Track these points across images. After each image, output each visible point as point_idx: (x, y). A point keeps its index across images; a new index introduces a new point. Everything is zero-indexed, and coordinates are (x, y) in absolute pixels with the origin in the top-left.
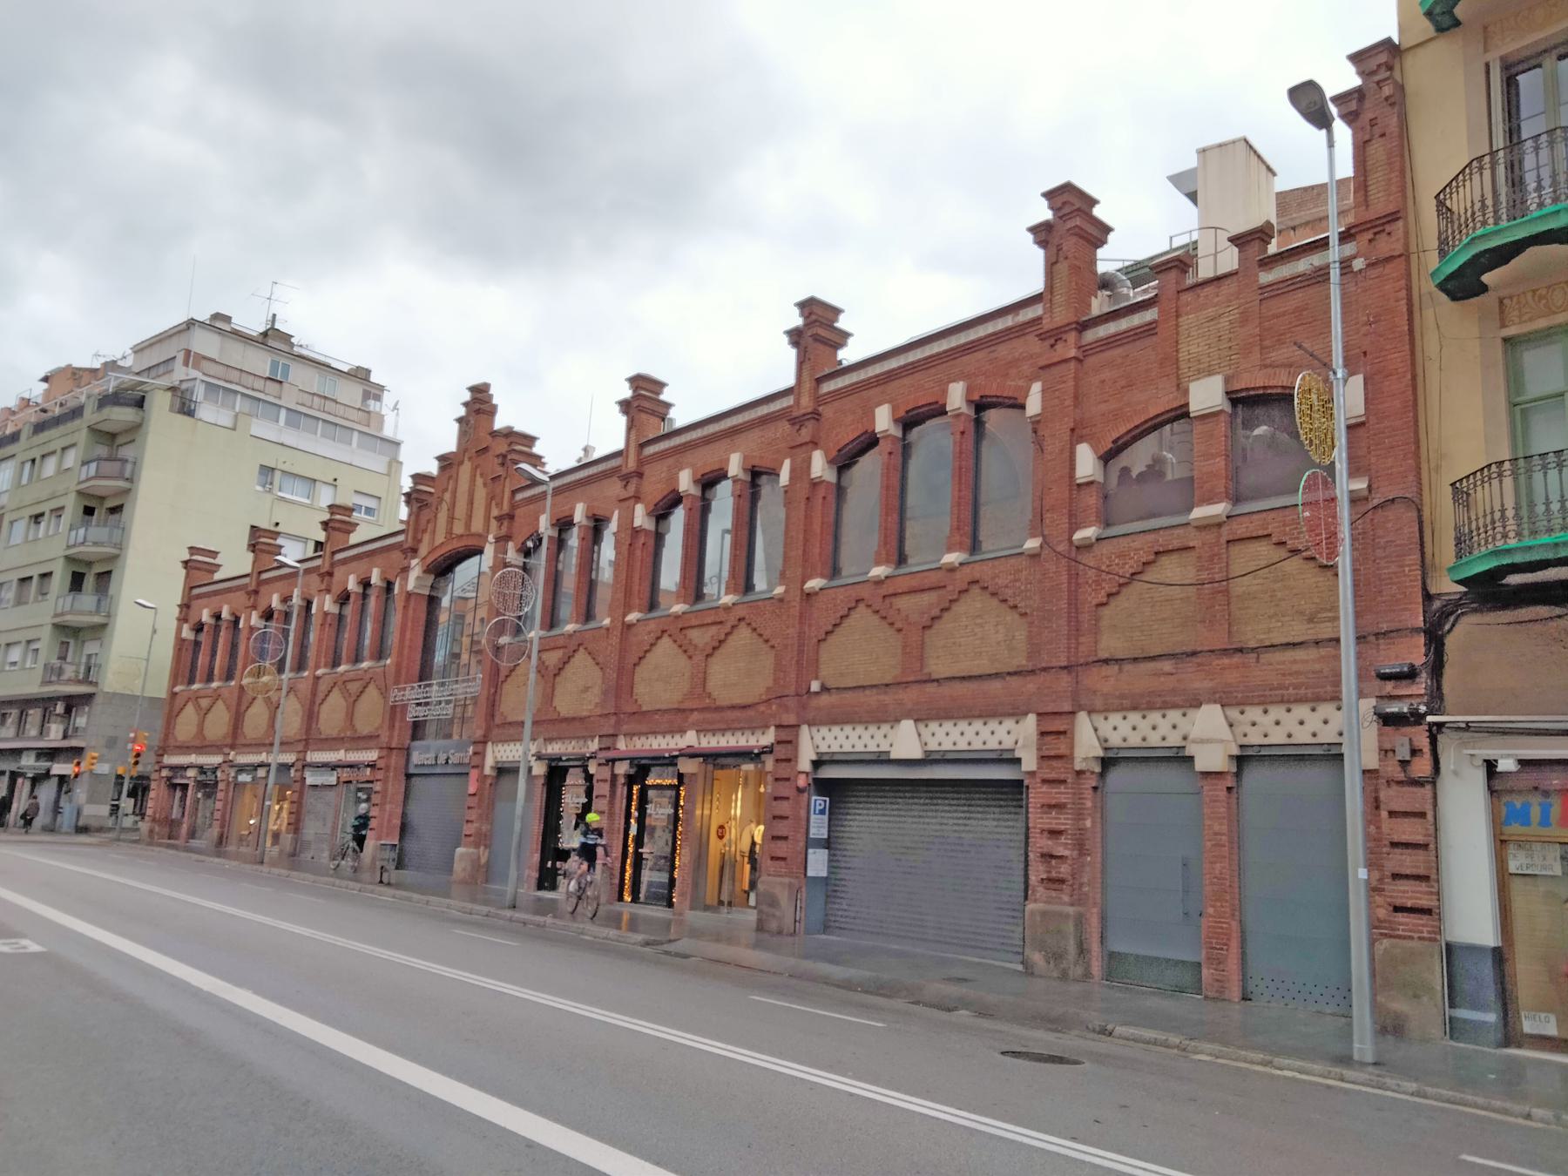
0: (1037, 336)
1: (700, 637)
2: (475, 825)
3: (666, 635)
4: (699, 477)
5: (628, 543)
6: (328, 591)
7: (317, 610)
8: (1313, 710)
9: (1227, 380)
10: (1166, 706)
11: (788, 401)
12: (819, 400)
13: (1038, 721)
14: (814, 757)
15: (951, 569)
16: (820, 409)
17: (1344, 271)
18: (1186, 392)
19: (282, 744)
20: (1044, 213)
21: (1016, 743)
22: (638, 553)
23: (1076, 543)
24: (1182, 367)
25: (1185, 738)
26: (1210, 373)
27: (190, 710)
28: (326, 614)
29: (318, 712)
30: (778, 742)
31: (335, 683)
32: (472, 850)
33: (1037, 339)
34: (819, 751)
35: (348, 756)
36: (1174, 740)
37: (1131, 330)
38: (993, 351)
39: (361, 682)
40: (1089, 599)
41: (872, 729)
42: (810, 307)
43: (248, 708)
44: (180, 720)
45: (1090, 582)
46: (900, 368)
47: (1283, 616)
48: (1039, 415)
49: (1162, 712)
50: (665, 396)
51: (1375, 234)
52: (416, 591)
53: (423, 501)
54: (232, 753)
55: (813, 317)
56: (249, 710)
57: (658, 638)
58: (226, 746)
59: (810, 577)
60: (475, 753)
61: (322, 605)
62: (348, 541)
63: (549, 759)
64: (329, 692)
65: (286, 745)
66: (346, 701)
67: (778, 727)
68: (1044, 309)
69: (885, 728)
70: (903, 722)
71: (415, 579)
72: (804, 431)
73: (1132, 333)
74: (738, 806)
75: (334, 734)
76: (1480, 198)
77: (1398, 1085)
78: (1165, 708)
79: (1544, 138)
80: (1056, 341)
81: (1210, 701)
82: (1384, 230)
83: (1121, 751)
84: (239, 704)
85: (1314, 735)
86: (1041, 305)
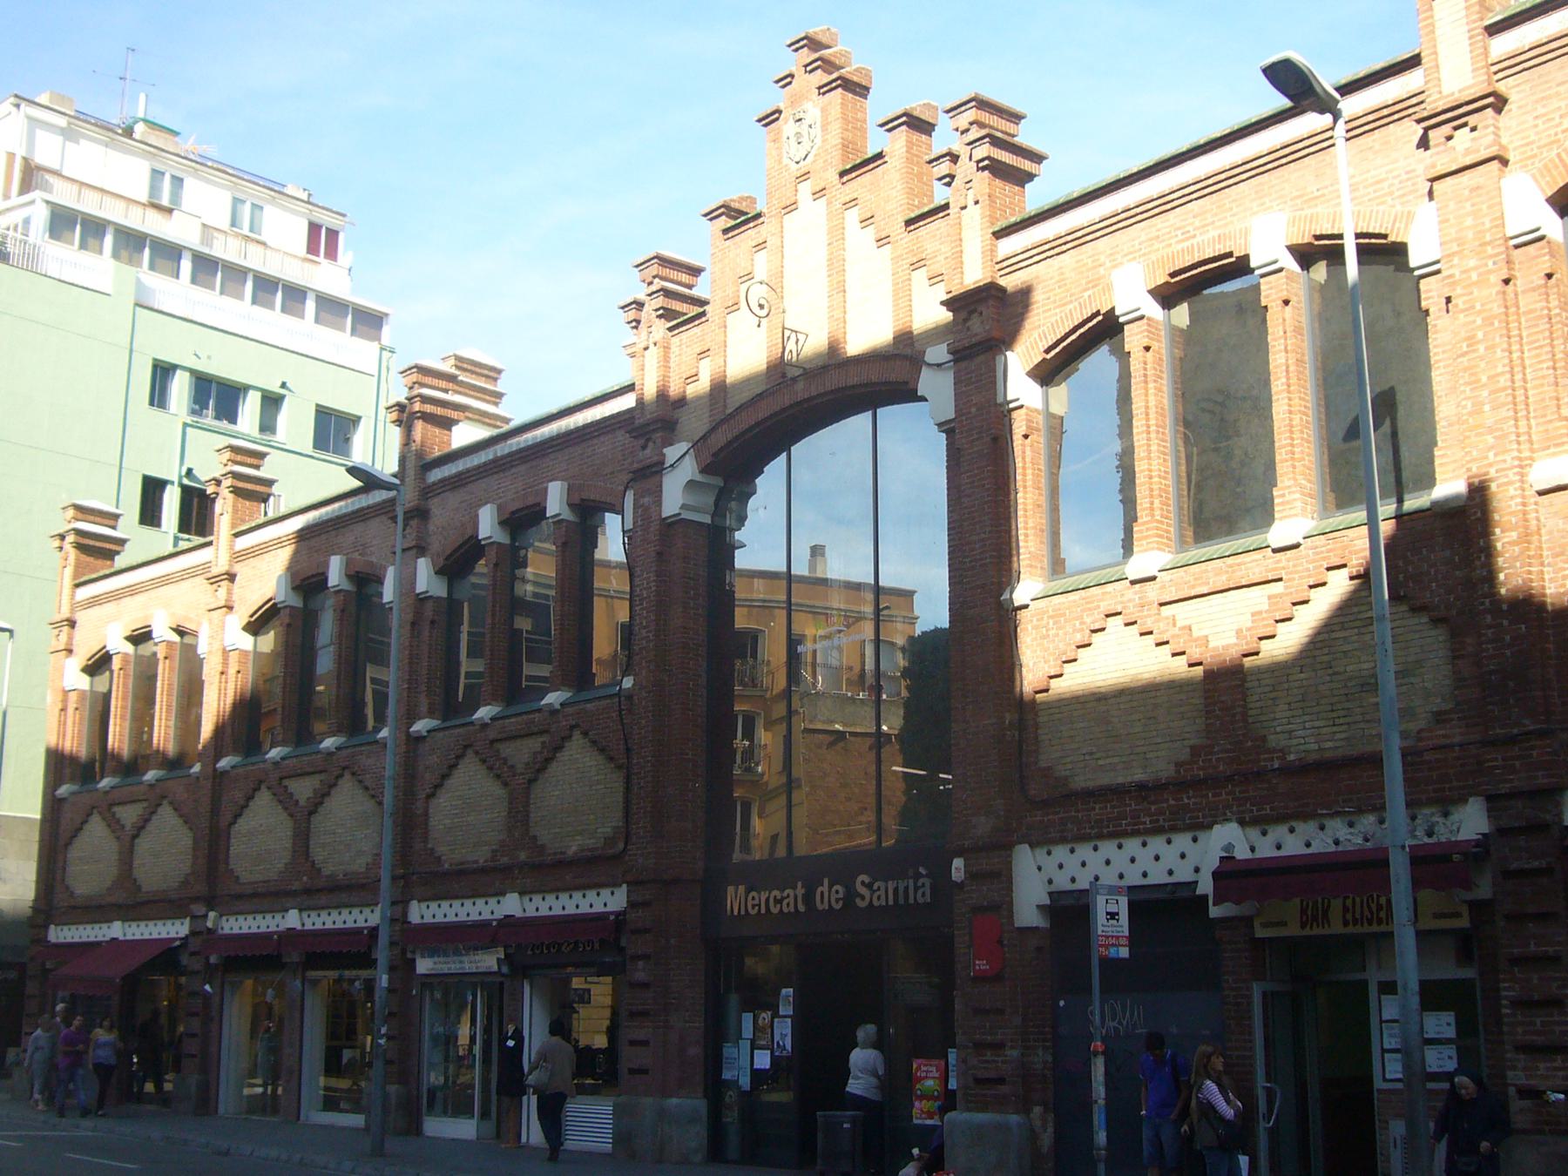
3: (470, 752)
4: (1162, 279)
6: (421, 549)
12: (427, 492)
27: (96, 828)
28: (422, 600)
29: (426, 814)
34: (1053, 888)
43: (237, 816)
44: (77, 851)
51: (1456, 128)
54: (212, 915)
56: (241, 821)
57: (459, 757)
58: (196, 899)
64: (453, 767)
74: (1536, 976)
75: (481, 856)
84: (215, 811)
85: (1170, 873)
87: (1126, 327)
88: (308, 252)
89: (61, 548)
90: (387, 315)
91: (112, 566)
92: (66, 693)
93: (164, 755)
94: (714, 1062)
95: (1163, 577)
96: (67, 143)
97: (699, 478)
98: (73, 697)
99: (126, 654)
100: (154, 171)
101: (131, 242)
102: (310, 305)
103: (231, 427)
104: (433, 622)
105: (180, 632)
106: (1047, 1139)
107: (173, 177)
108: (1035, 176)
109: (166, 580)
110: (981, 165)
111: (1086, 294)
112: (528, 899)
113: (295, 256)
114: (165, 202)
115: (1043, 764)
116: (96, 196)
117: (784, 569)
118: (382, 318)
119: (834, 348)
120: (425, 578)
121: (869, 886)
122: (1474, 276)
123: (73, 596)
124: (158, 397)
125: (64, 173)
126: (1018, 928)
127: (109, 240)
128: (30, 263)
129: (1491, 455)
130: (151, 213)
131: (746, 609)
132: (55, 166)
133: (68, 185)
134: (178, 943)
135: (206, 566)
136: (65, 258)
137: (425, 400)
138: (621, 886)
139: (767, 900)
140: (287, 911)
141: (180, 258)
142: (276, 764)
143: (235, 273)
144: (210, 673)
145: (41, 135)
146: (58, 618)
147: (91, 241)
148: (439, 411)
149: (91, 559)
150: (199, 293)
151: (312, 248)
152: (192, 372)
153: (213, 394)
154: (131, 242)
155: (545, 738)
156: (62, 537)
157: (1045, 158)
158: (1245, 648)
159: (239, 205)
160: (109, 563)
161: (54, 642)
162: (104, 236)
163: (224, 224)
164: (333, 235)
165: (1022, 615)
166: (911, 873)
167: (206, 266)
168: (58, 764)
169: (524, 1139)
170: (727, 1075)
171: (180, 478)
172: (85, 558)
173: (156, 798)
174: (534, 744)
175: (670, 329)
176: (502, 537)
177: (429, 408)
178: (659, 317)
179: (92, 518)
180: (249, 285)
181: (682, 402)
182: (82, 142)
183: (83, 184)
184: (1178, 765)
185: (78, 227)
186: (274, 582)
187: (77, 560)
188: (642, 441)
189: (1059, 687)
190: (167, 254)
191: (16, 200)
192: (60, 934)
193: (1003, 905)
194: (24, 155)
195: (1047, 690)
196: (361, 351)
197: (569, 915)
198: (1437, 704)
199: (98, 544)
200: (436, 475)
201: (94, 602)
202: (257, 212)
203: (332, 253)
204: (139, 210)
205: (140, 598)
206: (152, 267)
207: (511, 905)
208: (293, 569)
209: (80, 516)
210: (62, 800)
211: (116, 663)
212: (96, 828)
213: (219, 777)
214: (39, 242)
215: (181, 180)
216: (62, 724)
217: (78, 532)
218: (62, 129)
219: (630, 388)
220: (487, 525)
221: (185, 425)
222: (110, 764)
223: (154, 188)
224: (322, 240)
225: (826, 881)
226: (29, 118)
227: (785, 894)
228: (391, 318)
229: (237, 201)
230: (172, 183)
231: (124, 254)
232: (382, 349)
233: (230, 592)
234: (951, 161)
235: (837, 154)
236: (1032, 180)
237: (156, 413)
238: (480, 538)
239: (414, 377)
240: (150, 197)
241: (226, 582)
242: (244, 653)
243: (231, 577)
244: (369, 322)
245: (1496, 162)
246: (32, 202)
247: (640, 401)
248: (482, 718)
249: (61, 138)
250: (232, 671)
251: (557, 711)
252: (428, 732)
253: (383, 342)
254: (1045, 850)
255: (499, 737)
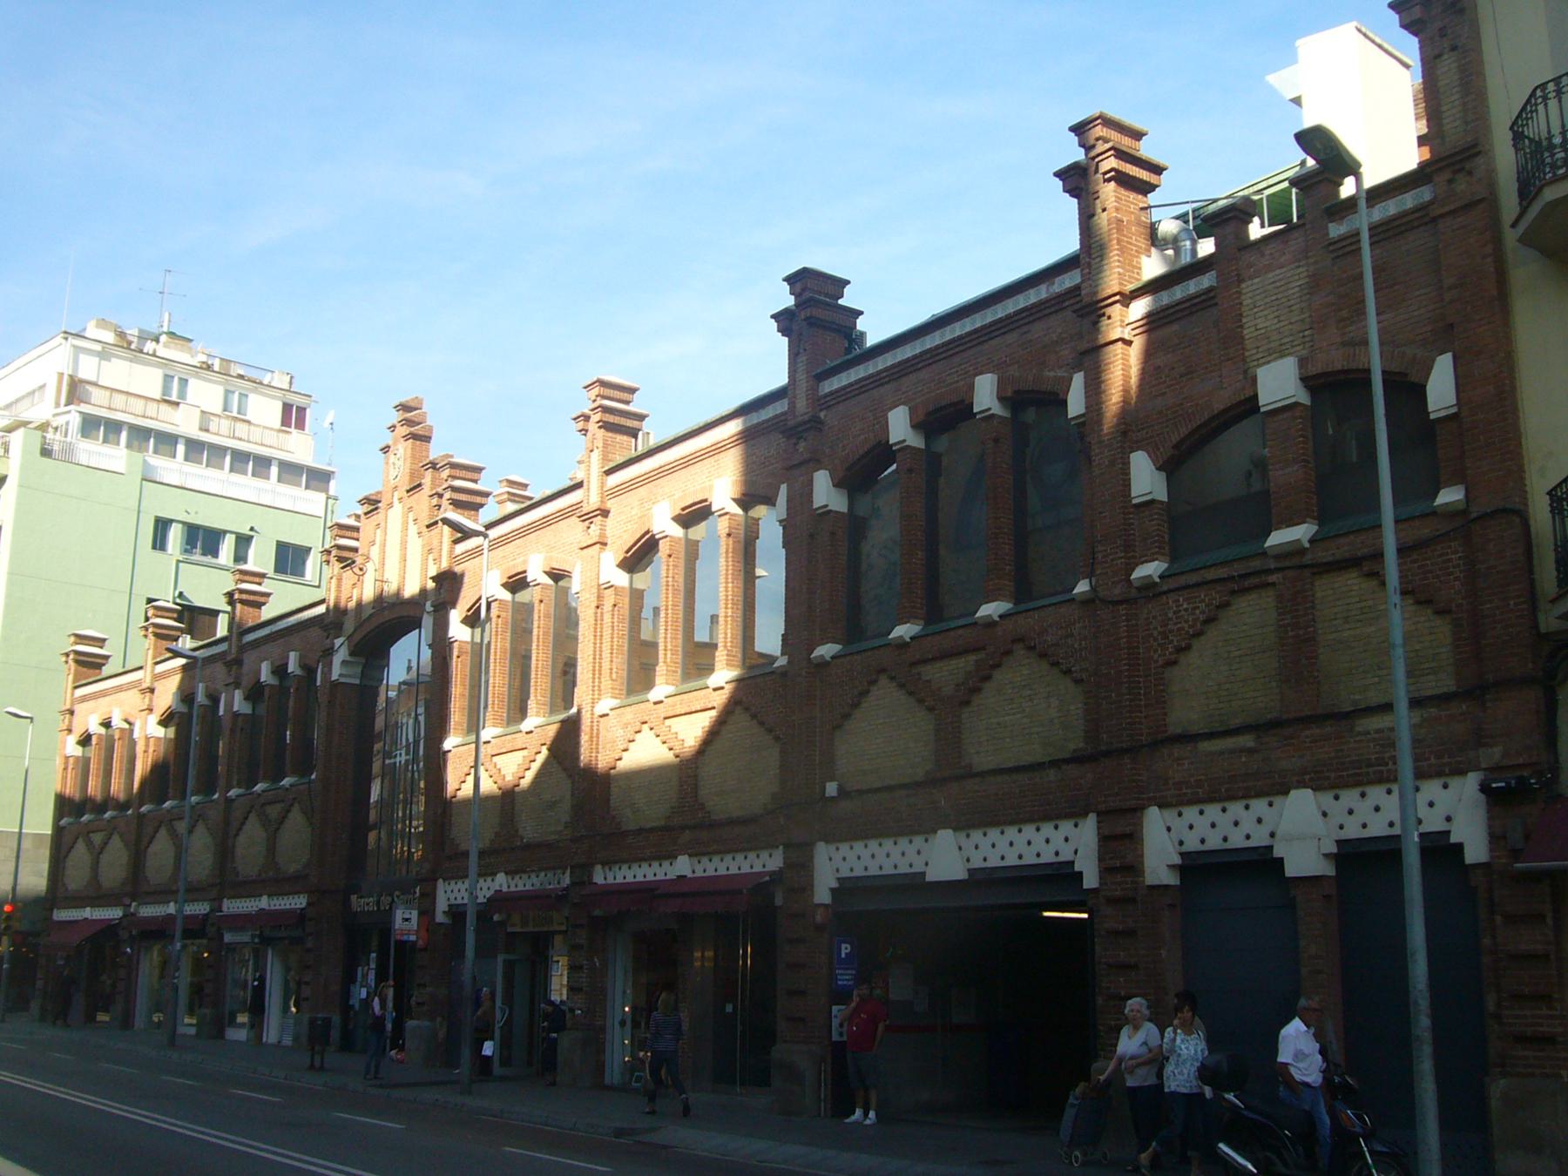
0: (1074, 312)
1: (946, 675)
2: (429, 989)
4: (678, 511)
5: (595, 604)
6: (237, 685)
7: (225, 711)
9: (1302, 363)
10: (1247, 794)
11: (780, 407)
12: (243, 648)
13: (1099, 822)
14: (834, 884)
16: (822, 415)
17: (1375, 239)
18: (1254, 380)
19: (188, 891)
21: (1076, 852)
22: (607, 618)
23: (1136, 584)
24: (1248, 347)
25: (1272, 835)
26: (1282, 355)
27: (81, 847)
28: (236, 715)
29: (234, 846)
31: (252, 807)
32: (427, 1023)
33: (1075, 315)
34: (1185, 849)
35: (272, 903)
36: (1259, 839)
37: (1188, 300)
38: (1029, 331)
39: (525, 753)
40: (1156, 656)
41: (903, 842)
42: (802, 281)
44: (70, 863)
45: (1155, 633)
46: (915, 357)
47: (1380, 668)
48: (1083, 415)
49: (1244, 802)
50: (848, 300)
52: (343, 680)
53: (347, 559)
54: (134, 904)
55: (807, 295)
60: (422, 895)
61: (230, 704)
62: (260, 617)
64: (246, 818)
65: (194, 891)
66: (266, 830)
67: (787, 846)
68: (1082, 276)
69: (918, 840)
70: (679, 857)
71: (339, 666)
72: (802, 446)
73: (1188, 304)
76: (1560, 130)
78: (928, 833)
79: (1551, 87)
81: (1301, 784)
82: (1463, 169)
86: (1078, 271)
87: (898, 455)
88: (282, 425)
89: (67, 662)
90: (333, 472)
91: (100, 673)
92: (67, 758)
93: (117, 801)
94: (346, 994)
95: (536, 731)
96: (103, 362)
97: (348, 658)
98: (71, 760)
99: (100, 735)
100: (166, 376)
101: (141, 435)
102: (274, 470)
103: (214, 561)
104: (242, 729)
105: (126, 721)
106: (442, 1034)
107: (180, 379)
108: (1158, 186)
109: (120, 689)
110: (1106, 177)
112: (834, 848)
113: (272, 429)
114: (174, 398)
115: (452, 837)
116: (123, 397)
118: (329, 475)
119: (398, 594)
120: (239, 703)
123: (73, 694)
124: (159, 543)
125: (100, 383)
126: (1149, 886)
127: (124, 435)
128: (68, 456)
130: (164, 407)
132: (93, 378)
133: (103, 392)
134: (767, 878)
135: (140, 681)
136: (93, 451)
137: (242, 591)
138: (777, 847)
140: (496, 875)
141: (176, 443)
142: (168, 811)
143: (217, 452)
144: (140, 748)
145: (82, 357)
146: (64, 709)
147: (111, 436)
148: (252, 598)
149: (85, 669)
150: (191, 468)
151: (286, 421)
152: (184, 523)
153: (200, 537)
154: (141, 435)
156: (67, 655)
157: (646, 416)
158: (610, 766)
159: (230, 395)
160: (97, 671)
161: (61, 725)
162: (121, 432)
163: (218, 409)
164: (302, 411)
165: (450, 755)
167: (195, 448)
168: (64, 805)
169: (264, 1040)
170: (351, 1003)
171: (174, 598)
172: (80, 668)
173: (111, 829)
174: (278, 807)
175: (343, 568)
176: (916, 441)
177: (244, 597)
178: (600, 427)
179: (87, 642)
180: (228, 459)
181: (345, 612)
182: (113, 360)
183: (113, 390)
185: (102, 428)
186: (171, 697)
187: (76, 670)
188: (794, 441)
189: (621, 765)
190: (166, 441)
191: (63, 409)
192: (61, 915)
193: (807, 887)
194: (70, 373)
195: (614, 768)
196: (313, 501)
197: (628, 883)
199: (89, 659)
201: (84, 699)
202: (244, 399)
203: (301, 425)
204: (155, 405)
205: (107, 698)
206: (156, 452)
207: (264, 903)
208: (181, 688)
209: (79, 641)
210: (63, 828)
211: (94, 740)
212: (81, 847)
213: (141, 818)
214: (74, 441)
215: (187, 380)
216: (64, 778)
217: (76, 652)
218: (99, 352)
219: (322, 602)
220: (900, 427)
221: (178, 561)
222: (88, 806)
223: (166, 389)
224: (293, 416)
226: (74, 346)
228: (336, 475)
229: (228, 393)
230: (180, 384)
231: (136, 443)
232: (328, 498)
233: (151, 700)
234: (584, 420)
235: (407, 482)
236: (1154, 190)
237: (158, 554)
238: (891, 442)
239: (237, 577)
240: (164, 395)
241: (148, 694)
242: (158, 739)
243: (152, 691)
244: (318, 478)
245: (1120, 343)
246: (69, 412)
247: (328, 609)
248: (901, 637)
249: (97, 359)
250: (151, 750)
251: (287, 789)
252: (1000, 616)
253: (332, 492)
254: (964, 834)
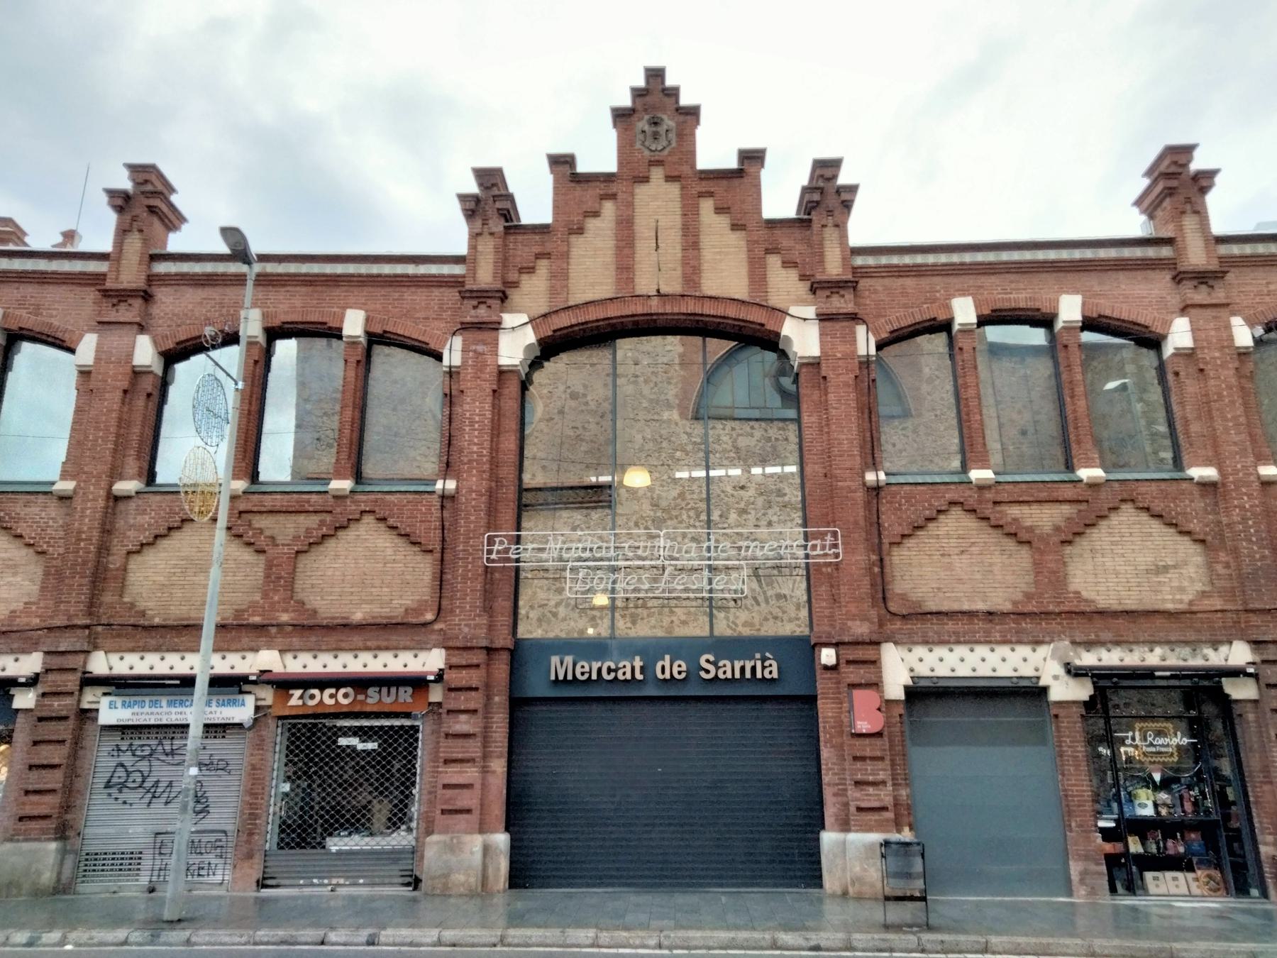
8: (315, 657)
12: (151, 279)
15: (339, 497)
20: (472, 188)
30: (451, 667)
51: (479, 303)
59: (121, 477)
63: (1093, 676)
77: (91, 938)
80: (479, 303)
83: (941, 681)
111: (925, 306)
117: (529, 326)
121: (715, 664)
122: (1219, 362)
129: (1238, 457)
131: (83, 246)
139: (599, 670)
155: (328, 518)
166: (758, 656)
184: (1015, 603)
198: (1199, 587)
200: (162, 268)
225: (667, 657)
227: (621, 665)
255: (255, 509)
